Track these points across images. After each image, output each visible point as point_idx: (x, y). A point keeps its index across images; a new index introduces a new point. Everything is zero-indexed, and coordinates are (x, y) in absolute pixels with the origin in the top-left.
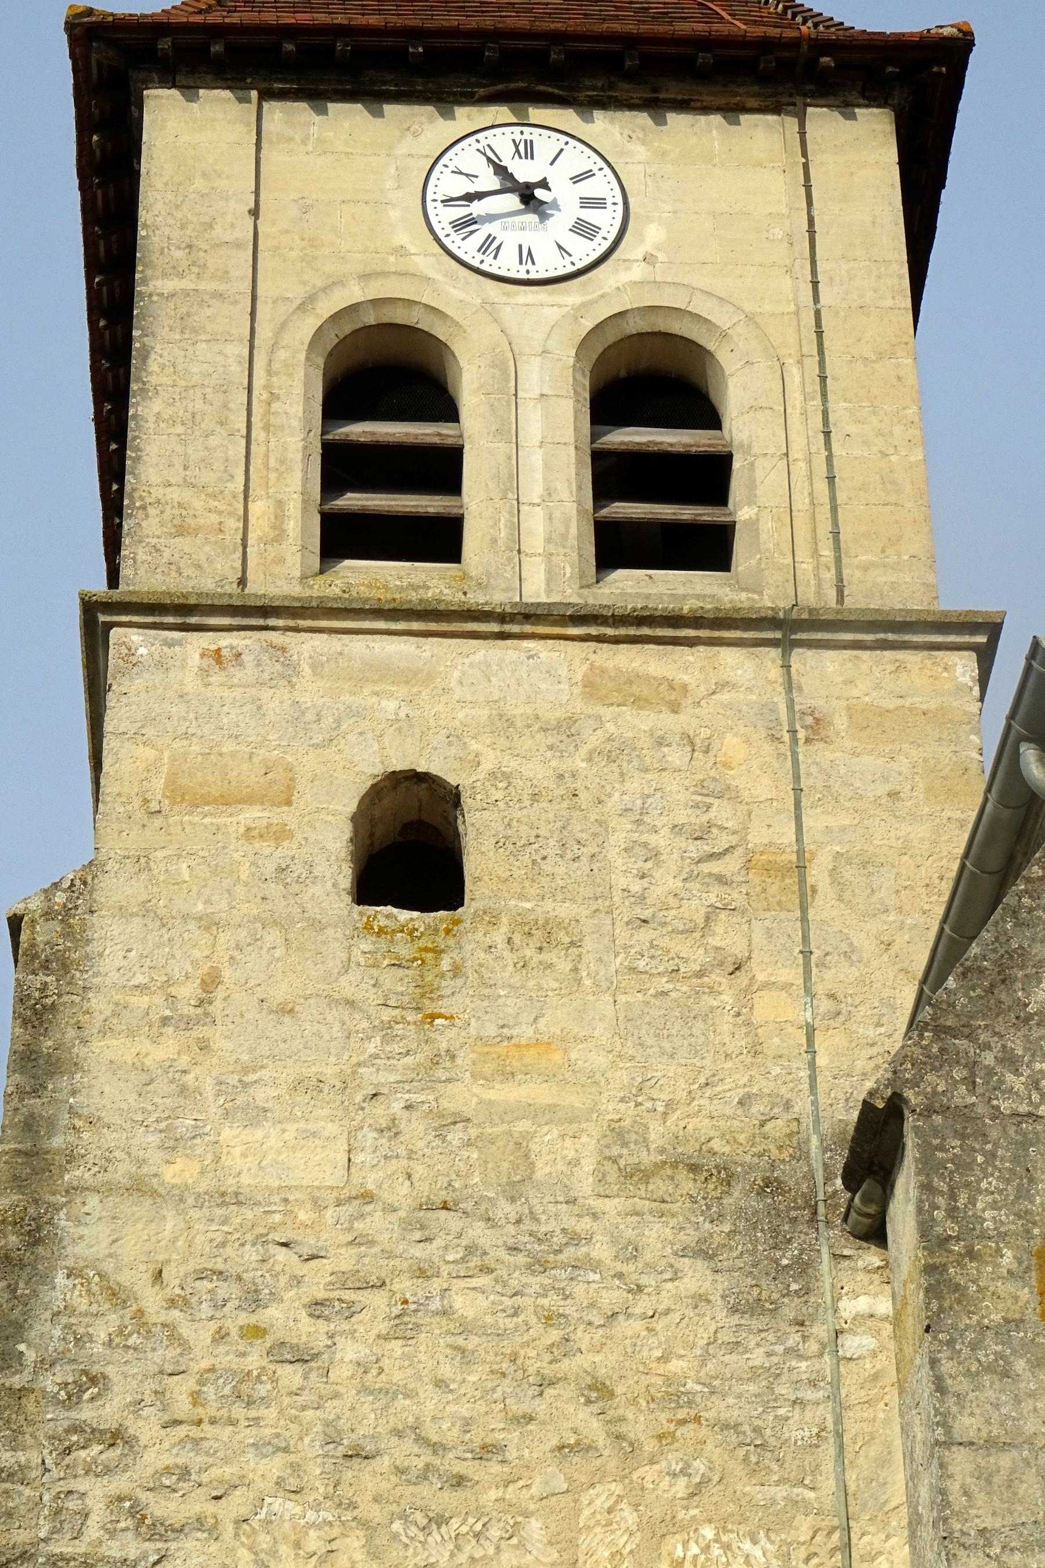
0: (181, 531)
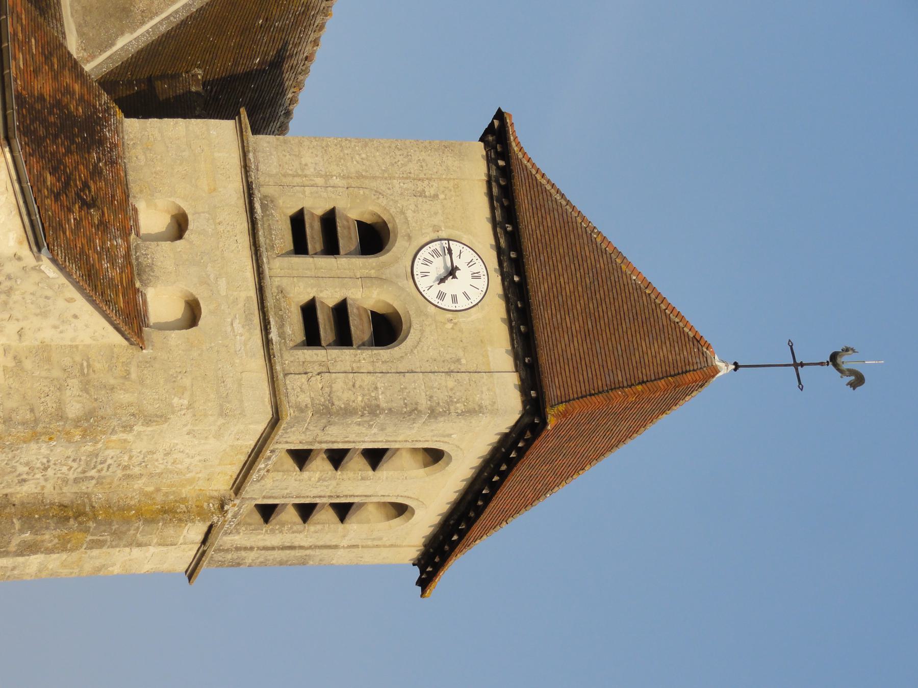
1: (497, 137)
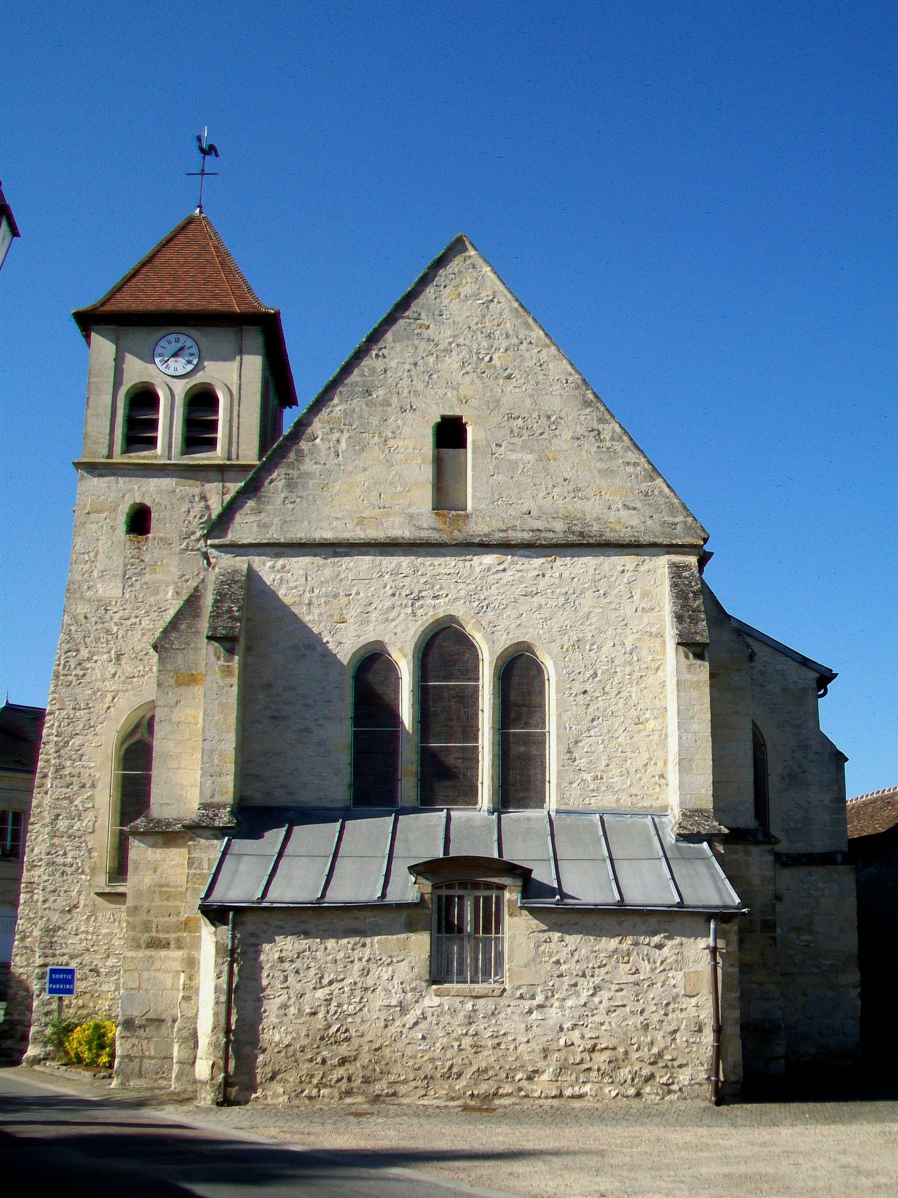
0: (95, 443)
1: (88, 321)
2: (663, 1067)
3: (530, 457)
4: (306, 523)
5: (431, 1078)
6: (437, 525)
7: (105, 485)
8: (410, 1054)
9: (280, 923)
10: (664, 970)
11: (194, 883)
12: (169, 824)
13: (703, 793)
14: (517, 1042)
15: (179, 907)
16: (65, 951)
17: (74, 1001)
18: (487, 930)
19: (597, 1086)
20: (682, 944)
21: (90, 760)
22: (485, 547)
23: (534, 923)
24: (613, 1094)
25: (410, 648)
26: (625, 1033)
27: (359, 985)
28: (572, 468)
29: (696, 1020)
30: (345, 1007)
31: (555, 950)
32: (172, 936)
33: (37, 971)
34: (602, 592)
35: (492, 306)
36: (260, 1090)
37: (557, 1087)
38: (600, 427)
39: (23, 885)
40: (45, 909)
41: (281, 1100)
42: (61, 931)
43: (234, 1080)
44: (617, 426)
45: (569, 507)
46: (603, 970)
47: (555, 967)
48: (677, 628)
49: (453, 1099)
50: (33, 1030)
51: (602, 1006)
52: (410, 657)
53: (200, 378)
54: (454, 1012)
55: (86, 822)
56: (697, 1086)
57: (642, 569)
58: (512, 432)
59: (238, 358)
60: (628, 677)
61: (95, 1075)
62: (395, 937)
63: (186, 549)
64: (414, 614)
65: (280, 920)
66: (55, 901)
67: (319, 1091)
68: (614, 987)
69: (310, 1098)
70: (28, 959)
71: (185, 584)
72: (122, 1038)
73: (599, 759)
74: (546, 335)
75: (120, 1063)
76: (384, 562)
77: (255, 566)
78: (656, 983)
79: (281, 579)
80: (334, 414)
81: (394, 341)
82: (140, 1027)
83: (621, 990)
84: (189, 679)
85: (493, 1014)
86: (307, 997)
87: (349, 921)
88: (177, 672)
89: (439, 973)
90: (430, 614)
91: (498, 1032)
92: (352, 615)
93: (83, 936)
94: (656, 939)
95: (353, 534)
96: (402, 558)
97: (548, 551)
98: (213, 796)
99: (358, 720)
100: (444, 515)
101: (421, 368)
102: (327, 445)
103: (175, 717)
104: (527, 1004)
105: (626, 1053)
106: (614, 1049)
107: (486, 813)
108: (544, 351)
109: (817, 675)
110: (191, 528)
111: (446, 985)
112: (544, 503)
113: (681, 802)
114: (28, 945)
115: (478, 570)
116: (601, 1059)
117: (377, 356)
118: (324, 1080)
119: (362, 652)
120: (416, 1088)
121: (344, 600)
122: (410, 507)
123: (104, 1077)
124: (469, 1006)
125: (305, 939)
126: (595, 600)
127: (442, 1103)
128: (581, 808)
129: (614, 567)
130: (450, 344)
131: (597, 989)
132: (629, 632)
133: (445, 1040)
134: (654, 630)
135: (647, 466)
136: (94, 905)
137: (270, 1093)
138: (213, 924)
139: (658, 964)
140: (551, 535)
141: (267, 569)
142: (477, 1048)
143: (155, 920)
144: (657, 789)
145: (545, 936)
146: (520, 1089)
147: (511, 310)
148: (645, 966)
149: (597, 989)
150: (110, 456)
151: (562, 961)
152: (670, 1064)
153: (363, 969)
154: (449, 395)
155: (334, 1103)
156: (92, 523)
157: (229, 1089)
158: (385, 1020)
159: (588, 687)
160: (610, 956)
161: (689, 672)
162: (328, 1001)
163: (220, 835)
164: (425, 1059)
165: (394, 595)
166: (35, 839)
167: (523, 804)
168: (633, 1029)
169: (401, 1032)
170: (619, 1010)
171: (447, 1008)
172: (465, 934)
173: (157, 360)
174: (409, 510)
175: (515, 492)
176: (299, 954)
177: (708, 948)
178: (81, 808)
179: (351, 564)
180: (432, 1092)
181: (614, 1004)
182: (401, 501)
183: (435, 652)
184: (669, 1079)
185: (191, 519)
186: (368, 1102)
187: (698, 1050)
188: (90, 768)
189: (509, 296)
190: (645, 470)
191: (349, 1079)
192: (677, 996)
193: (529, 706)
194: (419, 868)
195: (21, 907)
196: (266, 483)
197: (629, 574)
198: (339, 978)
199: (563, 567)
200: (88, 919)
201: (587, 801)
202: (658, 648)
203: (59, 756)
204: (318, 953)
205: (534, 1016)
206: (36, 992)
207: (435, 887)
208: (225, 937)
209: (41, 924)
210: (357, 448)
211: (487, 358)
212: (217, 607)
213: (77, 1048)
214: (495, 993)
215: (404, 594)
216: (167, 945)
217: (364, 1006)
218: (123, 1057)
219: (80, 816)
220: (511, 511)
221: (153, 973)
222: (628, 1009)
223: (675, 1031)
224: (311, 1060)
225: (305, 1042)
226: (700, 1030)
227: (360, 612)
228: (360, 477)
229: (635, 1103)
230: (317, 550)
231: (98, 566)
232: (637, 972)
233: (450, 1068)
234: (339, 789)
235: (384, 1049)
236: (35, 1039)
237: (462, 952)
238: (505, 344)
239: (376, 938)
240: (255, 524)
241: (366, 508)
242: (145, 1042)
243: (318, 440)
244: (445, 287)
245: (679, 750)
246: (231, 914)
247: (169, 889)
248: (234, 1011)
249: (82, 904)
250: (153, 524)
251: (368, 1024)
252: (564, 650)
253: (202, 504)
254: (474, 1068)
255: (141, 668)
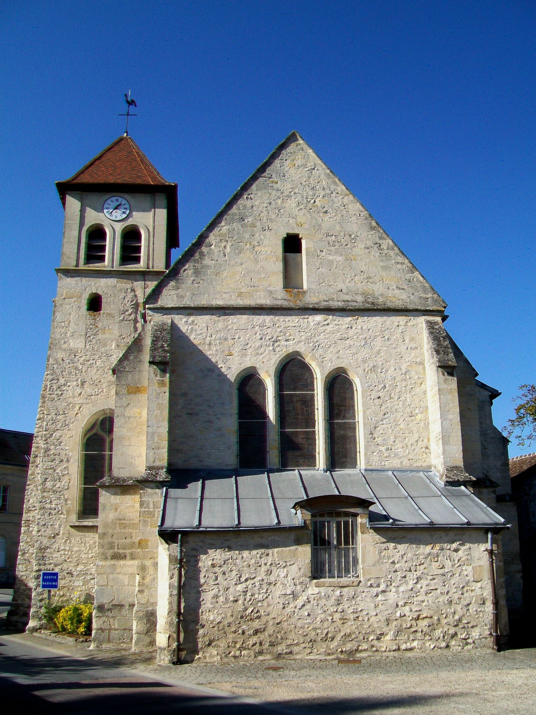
2: (462, 628)
3: (339, 258)
4: (206, 295)
5: (315, 641)
6: (286, 297)
7: (74, 282)
8: (300, 626)
9: (212, 541)
10: (460, 565)
11: (144, 517)
12: (124, 481)
13: (457, 457)
14: (369, 615)
15: (131, 533)
16: (51, 561)
17: (58, 593)
18: (347, 543)
19: (421, 642)
20: (470, 549)
21: (65, 445)
22: (315, 310)
23: (377, 537)
24: (432, 647)
25: (272, 371)
26: (438, 607)
27: (265, 581)
28: (365, 265)
29: (481, 597)
30: (256, 596)
31: (391, 555)
32: (128, 552)
33: (34, 574)
34: (386, 337)
35: (314, 172)
36: (201, 653)
37: (397, 644)
38: (381, 242)
39: (23, 522)
40: (39, 536)
41: (215, 659)
42: (49, 549)
43: (184, 647)
44: (391, 241)
45: (365, 288)
46: (422, 567)
47: (392, 566)
48: (437, 357)
49: (329, 654)
50: (32, 610)
51: (422, 590)
52: (273, 376)
53: (130, 222)
54: (328, 597)
55: (63, 482)
56: (484, 639)
57: (409, 324)
58: (329, 243)
59: (153, 210)
60: (404, 388)
61: (76, 640)
62: (288, 548)
63: (123, 320)
64: (274, 350)
65: (211, 540)
66: (45, 531)
67: (241, 653)
68: (430, 577)
69: (235, 657)
70: (26, 567)
71: (122, 340)
72: (97, 617)
73: (389, 438)
74: (347, 188)
75: (96, 633)
76: (255, 319)
77: (176, 321)
78: (455, 574)
79: (192, 329)
80: (222, 232)
81: (257, 190)
82: (108, 610)
83: (434, 579)
84: (136, 390)
85: (353, 597)
86: (231, 590)
87: (257, 539)
88: (128, 385)
89: (317, 572)
90: (284, 351)
91: (357, 609)
92: (236, 351)
93: (62, 552)
94: (454, 546)
95: (235, 302)
96: (266, 317)
97: (354, 313)
98: (154, 462)
99: (241, 415)
100: (290, 292)
101: (273, 206)
102: (218, 249)
103: (127, 414)
104: (375, 590)
105: (439, 620)
106: (431, 617)
107: (322, 472)
108: (346, 198)
109: (490, 394)
110: (126, 308)
111: (322, 580)
112: (350, 285)
113: (444, 462)
114: (26, 558)
115: (312, 324)
116: (423, 624)
117: (247, 198)
118: (244, 645)
119: (243, 374)
120: (305, 648)
121: (231, 342)
122: (270, 286)
123: (82, 642)
124: (338, 593)
125: (229, 551)
126: (383, 342)
127: (322, 657)
128: (379, 468)
129: (393, 322)
130: (290, 192)
131: (419, 579)
132: (404, 361)
133: (323, 616)
134: (418, 360)
135: (409, 265)
136: (69, 533)
137: (208, 655)
138: (167, 543)
139: (456, 562)
140: (355, 304)
141: (183, 323)
142: (344, 620)
143: (116, 541)
144: (425, 456)
145: (385, 545)
146: (373, 646)
147: (325, 174)
148: (448, 563)
149: (419, 579)
150: (77, 265)
151: (396, 562)
152: (466, 625)
153: (268, 571)
154: (291, 221)
155: (251, 660)
156: (67, 304)
157: (181, 653)
158: (283, 604)
159: (380, 394)
160: (426, 558)
161: (445, 383)
162: (245, 592)
163: (160, 486)
164: (310, 628)
165: (261, 339)
166: (31, 494)
167: (343, 466)
168: (443, 604)
169: (294, 611)
170: (433, 592)
171: (323, 595)
172: (332, 546)
173: (105, 211)
174: (269, 288)
175: (332, 278)
176: (225, 561)
177: (487, 550)
178: (60, 474)
179: (235, 320)
180: (315, 651)
181: (430, 589)
182: (264, 283)
183: (287, 373)
184: (466, 636)
185: (126, 302)
186: (274, 659)
187: (483, 616)
188: (66, 450)
189: (324, 166)
190: (408, 267)
191: (261, 644)
192: (469, 582)
193: (345, 406)
194: (303, 503)
195: (22, 535)
196: (182, 271)
197: (402, 327)
198: (252, 577)
199: (363, 323)
200: (66, 541)
201: (383, 463)
202: (421, 371)
203: (47, 443)
204: (237, 561)
205: (380, 598)
206: (34, 587)
207: (313, 516)
208: (175, 551)
209: (37, 545)
210: (237, 251)
211: (312, 201)
212: (155, 344)
213: (62, 622)
214: (354, 584)
215: (267, 338)
216: (124, 557)
217: (269, 595)
218: (98, 630)
219: (60, 479)
220: (330, 289)
221: (116, 575)
222: (439, 591)
223: (469, 605)
224: (235, 632)
225: (230, 620)
226: (484, 603)
227: (243, 349)
228: (239, 269)
229: (446, 652)
230: (214, 312)
231: (70, 329)
232: (443, 567)
233: (327, 634)
234: (231, 458)
235: (283, 623)
236: (33, 616)
237: (331, 557)
238: (322, 193)
239: (276, 550)
240: (175, 296)
241: (243, 287)
242: (112, 620)
243: (213, 247)
244: (286, 160)
245: (442, 430)
246: (180, 536)
247: (125, 522)
248: (183, 600)
249: (61, 533)
250: (103, 305)
251: (272, 607)
252: (366, 372)
253: (133, 294)
254: (342, 633)
255: (96, 390)
